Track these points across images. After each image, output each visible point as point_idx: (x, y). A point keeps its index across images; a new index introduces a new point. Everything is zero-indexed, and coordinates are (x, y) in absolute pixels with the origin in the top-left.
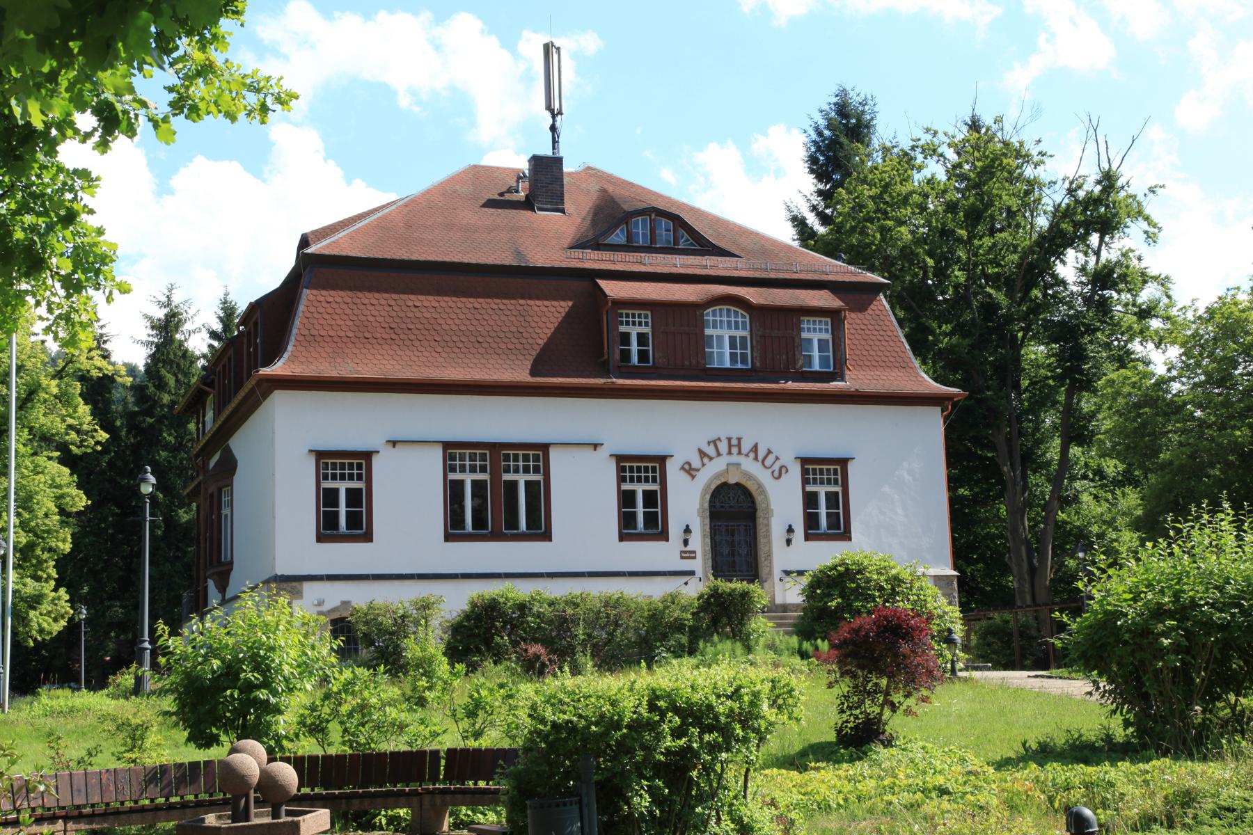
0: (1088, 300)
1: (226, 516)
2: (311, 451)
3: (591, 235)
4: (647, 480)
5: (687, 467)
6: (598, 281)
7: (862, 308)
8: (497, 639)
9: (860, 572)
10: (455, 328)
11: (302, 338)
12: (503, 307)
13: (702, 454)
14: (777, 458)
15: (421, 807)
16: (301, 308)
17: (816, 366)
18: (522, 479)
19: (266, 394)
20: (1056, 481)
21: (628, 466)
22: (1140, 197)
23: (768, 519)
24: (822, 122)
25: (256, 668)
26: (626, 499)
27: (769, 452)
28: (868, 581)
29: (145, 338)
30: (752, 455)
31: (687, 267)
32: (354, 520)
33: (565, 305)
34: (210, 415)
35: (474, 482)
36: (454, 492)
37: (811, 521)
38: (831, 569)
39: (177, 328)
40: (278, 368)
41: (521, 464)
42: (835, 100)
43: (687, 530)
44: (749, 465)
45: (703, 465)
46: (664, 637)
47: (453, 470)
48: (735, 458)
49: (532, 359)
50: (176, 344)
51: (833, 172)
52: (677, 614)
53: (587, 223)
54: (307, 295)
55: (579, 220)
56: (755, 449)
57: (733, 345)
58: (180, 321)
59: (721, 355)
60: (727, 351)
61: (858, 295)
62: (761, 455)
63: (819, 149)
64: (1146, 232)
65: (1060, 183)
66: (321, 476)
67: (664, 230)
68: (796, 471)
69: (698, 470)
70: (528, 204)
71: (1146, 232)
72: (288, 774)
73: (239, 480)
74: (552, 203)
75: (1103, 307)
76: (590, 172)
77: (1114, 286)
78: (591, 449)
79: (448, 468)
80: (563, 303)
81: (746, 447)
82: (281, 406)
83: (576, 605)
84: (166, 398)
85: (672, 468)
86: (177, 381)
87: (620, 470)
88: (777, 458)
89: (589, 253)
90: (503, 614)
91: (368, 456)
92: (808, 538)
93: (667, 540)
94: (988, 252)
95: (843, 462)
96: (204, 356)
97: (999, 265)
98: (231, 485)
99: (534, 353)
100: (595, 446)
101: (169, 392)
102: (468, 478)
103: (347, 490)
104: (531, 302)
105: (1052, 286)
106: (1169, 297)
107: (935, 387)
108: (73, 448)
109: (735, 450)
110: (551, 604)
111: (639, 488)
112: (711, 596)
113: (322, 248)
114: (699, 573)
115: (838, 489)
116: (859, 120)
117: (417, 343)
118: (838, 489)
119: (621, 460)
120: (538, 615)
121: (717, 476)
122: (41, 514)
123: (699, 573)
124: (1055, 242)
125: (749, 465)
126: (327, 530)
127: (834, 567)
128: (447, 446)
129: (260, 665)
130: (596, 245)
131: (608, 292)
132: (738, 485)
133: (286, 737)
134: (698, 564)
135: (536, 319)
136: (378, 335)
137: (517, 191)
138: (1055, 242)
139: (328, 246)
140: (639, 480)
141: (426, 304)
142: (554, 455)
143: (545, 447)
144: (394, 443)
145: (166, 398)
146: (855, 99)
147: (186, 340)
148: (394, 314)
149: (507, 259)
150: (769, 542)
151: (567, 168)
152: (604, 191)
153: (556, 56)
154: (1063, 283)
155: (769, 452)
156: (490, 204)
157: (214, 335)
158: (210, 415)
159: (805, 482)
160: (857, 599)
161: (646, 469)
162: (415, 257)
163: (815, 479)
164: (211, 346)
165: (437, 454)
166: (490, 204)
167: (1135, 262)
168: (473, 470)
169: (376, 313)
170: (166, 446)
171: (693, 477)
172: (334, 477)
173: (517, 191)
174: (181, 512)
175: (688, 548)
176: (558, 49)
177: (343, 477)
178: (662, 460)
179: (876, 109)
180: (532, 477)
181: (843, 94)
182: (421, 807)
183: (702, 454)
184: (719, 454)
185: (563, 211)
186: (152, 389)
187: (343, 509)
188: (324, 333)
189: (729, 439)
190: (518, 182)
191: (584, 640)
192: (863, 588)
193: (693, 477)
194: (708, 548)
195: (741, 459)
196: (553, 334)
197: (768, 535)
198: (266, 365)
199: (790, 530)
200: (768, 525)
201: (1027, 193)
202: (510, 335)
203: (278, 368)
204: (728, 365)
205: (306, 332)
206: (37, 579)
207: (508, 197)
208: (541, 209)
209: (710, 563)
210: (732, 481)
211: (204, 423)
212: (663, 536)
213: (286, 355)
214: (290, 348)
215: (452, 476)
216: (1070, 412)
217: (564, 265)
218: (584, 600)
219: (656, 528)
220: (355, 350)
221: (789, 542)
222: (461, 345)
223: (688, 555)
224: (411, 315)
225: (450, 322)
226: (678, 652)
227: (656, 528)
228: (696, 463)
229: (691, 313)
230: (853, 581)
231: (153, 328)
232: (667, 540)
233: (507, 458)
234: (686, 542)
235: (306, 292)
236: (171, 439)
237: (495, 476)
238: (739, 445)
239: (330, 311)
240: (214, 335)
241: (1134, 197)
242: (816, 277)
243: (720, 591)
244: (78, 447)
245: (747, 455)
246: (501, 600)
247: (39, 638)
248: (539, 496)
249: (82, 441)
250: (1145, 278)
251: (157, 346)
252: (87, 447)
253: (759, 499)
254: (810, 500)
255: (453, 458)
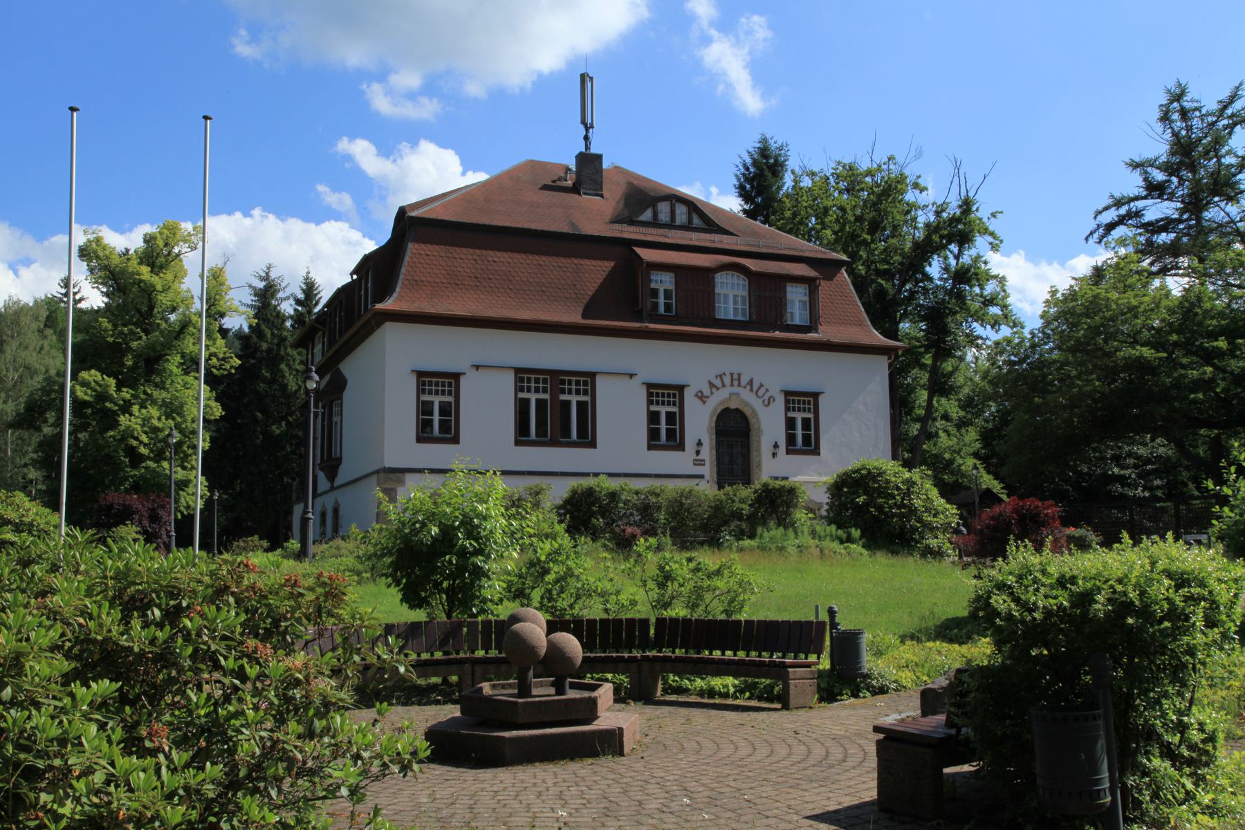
0: (950, 293)
1: (336, 423)
2: (413, 371)
3: (626, 213)
4: (669, 404)
5: (700, 394)
6: (635, 248)
7: (830, 277)
8: (594, 521)
9: (880, 475)
10: (524, 279)
11: (407, 282)
12: (561, 265)
13: (711, 385)
14: (767, 390)
15: (640, 672)
16: (407, 258)
17: (797, 321)
18: (574, 399)
19: (379, 325)
20: (923, 420)
21: (655, 391)
22: (985, 220)
23: (759, 437)
24: (749, 161)
25: (469, 535)
26: (653, 418)
27: (761, 385)
28: (888, 482)
29: (250, 303)
30: (748, 387)
31: (700, 240)
32: (445, 426)
33: (609, 265)
34: (318, 348)
35: (538, 401)
36: (522, 408)
37: (791, 440)
38: (854, 473)
39: (273, 295)
40: (389, 304)
41: (574, 387)
42: (758, 145)
43: (699, 443)
44: (746, 395)
45: (712, 393)
46: (726, 523)
47: (522, 390)
48: (736, 389)
49: (583, 306)
50: (271, 307)
51: (756, 196)
52: (736, 505)
53: (621, 205)
54: (411, 247)
55: (614, 204)
56: (751, 382)
57: (735, 302)
58: (275, 291)
59: (726, 308)
60: (731, 305)
61: (827, 268)
62: (755, 387)
63: (747, 179)
64: (991, 244)
65: (930, 206)
66: (420, 390)
67: (681, 212)
68: (780, 400)
69: (708, 397)
70: (575, 189)
71: (991, 244)
72: (571, 643)
73: (348, 395)
74: (594, 190)
75: (960, 297)
76: (617, 169)
77: (968, 281)
78: (628, 377)
79: (518, 389)
80: (606, 263)
81: (744, 381)
82: (390, 333)
83: (658, 495)
84: (264, 346)
85: (689, 396)
86: (273, 334)
87: (650, 395)
88: (767, 390)
89: (626, 228)
90: (598, 500)
91: (456, 376)
92: (788, 452)
93: (684, 450)
94: (881, 253)
95: (816, 395)
96: (291, 317)
97: (888, 263)
98: (341, 398)
99: (585, 302)
100: (631, 376)
101: (267, 342)
102: (533, 397)
103: (440, 402)
104: (582, 261)
105: (922, 281)
106: (1004, 291)
107: (879, 339)
108: (214, 370)
109: (736, 383)
110: (637, 493)
111: (663, 410)
112: (763, 491)
113: (425, 212)
114: (707, 476)
115: (811, 416)
116: (776, 160)
117: (496, 290)
118: (811, 416)
119: (650, 386)
120: (626, 502)
121: (723, 402)
122: (189, 419)
123: (707, 476)
124: (925, 249)
125: (746, 395)
126: (424, 434)
127: (857, 471)
128: (518, 371)
129: (472, 532)
130: (632, 222)
131: (642, 256)
132: (737, 410)
133: (491, 601)
134: (708, 470)
135: (587, 275)
136: (466, 283)
137: (566, 180)
138: (925, 249)
139: (426, 212)
140: (663, 403)
141: (503, 260)
142: (600, 381)
143: (592, 375)
144: (477, 367)
145: (264, 346)
146: (773, 146)
147: (279, 305)
148: (478, 267)
149: (565, 228)
150: (760, 455)
151: (605, 165)
152: (630, 184)
153: (589, 84)
154: (931, 279)
155: (761, 385)
156: (545, 187)
157: (298, 302)
158: (318, 348)
159: (787, 409)
160: (879, 497)
161: (669, 395)
162: (494, 223)
163: (804, 409)
164: (296, 310)
165: (510, 377)
166: (545, 187)
167: (983, 266)
168: (537, 390)
169: (464, 265)
170: (265, 380)
171: (704, 402)
172: (430, 393)
173: (566, 180)
174: (274, 427)
175: (700, 457)
176: (591, 79)
177: (437, 393)
178: (681, 388)
179: (789, 153)
180: (582, 398)
181: (764, 141)
182: (640, 672)
183: (711, 385)
184: (724, 386)
185: (602, 196)
186: (255, 339)
187: (436, 418)
188: (424, 279)
189: (732, 374)
190: (566, 173)
191: (664, 524)
192: (884, 488)
193: (704, 402)
194: (714, 458)
195: (740, 390)
196: (599, 287)
197: (759, 450)
198: (380, 302)
199: (776, 446)
200: (759, 442)
201: (908, 212)
202: (567, 287)
203: (389, 304)
204: (731, 317)
205: (410, 278)
206: (184, 468)
207: (559, 183)
208: (585, 194)
209: (715, 469)
210: (733, 406)
211: (313, 354)
212: (681, 447)
213: (395, 295)
214: (398, 289)
215: (521, 395)
216: (934, 371)
217: (608, 235)
218: (662, 491)
219: (675, 441)
220: (448, 294)
221: (774, 455)
222: (529, 293)
223: (699, 463)
224: (491, 268)
225: (521, 275)
226: (740, 535)
227: (675, 441)
228: (707, 392)
229: (706, 275)
230: (876, 481)
231: (255, 295)
232: (684, 450)
233: (563, 382)
234: (698, 453)
235: (410, 245)
236: (268, 375)
237: (554, 397)
238: (739, 379)
239: (429, 262)
240: (298, 302)
241: (980, 219)
242: (796, 253)
243: (770, 487)
244: (218, 370)
245: (745, 387)
246: (597, 489)
247: (185, 513)
248: (587, 413)
249: (221, 365)
250: (989, 276)
251: (259, 308)
252: (225, 369)
253: (752, 421)
254: (790, 423)
255: (522, 380)
